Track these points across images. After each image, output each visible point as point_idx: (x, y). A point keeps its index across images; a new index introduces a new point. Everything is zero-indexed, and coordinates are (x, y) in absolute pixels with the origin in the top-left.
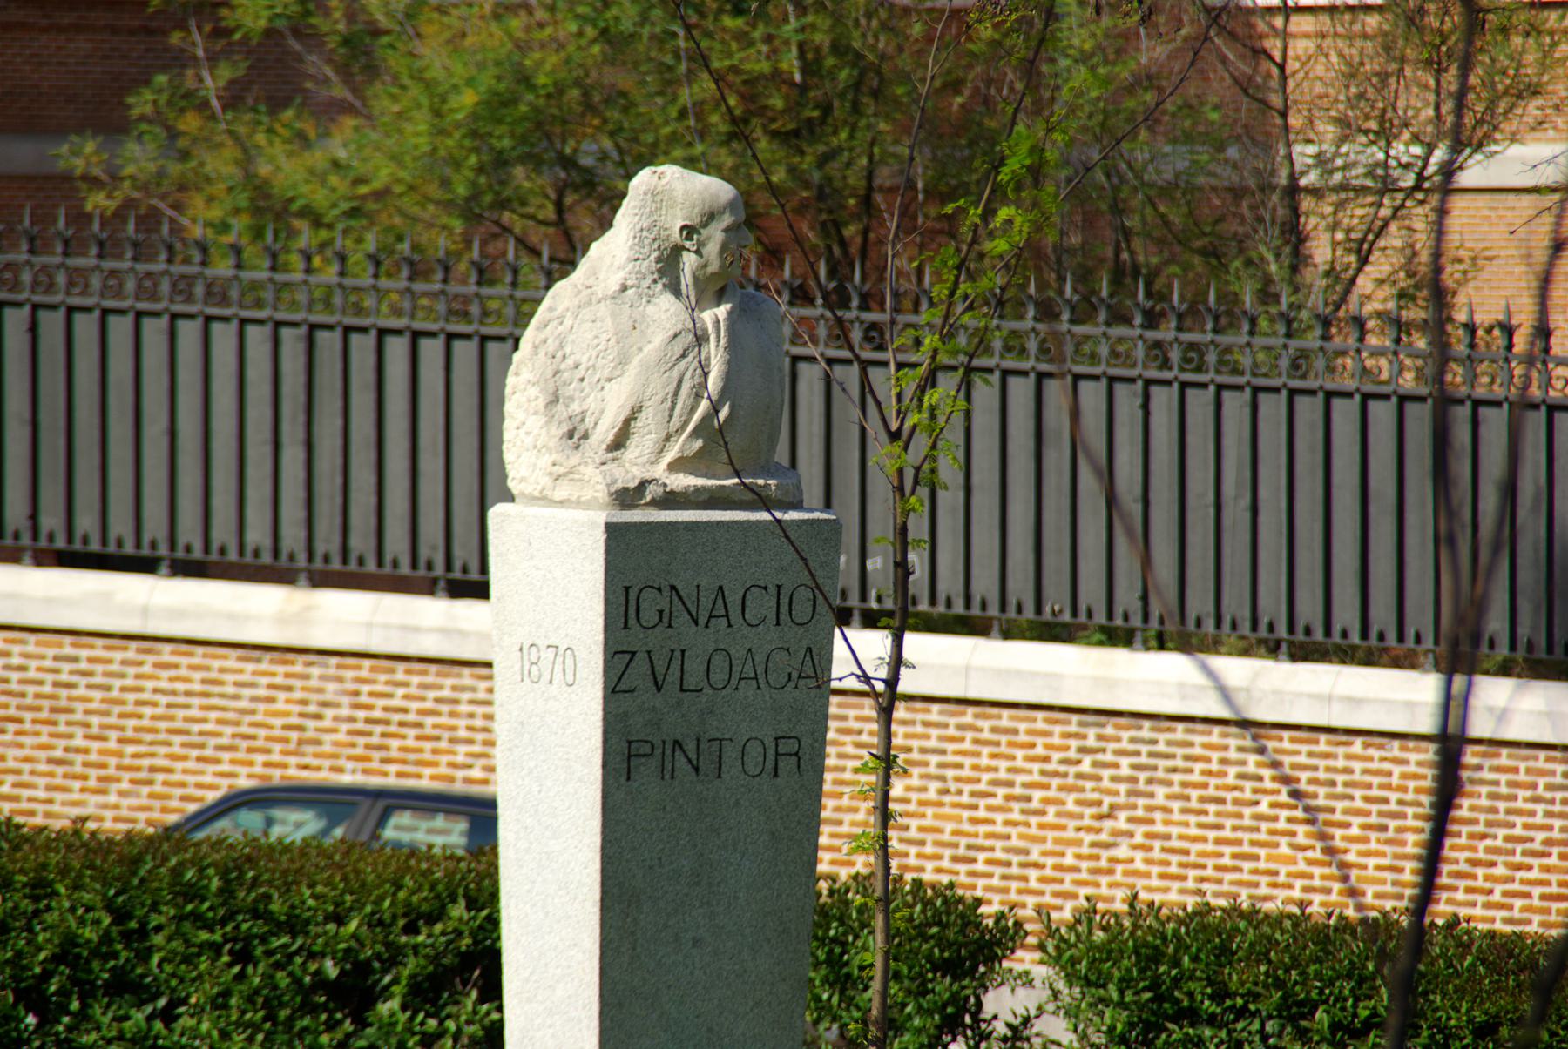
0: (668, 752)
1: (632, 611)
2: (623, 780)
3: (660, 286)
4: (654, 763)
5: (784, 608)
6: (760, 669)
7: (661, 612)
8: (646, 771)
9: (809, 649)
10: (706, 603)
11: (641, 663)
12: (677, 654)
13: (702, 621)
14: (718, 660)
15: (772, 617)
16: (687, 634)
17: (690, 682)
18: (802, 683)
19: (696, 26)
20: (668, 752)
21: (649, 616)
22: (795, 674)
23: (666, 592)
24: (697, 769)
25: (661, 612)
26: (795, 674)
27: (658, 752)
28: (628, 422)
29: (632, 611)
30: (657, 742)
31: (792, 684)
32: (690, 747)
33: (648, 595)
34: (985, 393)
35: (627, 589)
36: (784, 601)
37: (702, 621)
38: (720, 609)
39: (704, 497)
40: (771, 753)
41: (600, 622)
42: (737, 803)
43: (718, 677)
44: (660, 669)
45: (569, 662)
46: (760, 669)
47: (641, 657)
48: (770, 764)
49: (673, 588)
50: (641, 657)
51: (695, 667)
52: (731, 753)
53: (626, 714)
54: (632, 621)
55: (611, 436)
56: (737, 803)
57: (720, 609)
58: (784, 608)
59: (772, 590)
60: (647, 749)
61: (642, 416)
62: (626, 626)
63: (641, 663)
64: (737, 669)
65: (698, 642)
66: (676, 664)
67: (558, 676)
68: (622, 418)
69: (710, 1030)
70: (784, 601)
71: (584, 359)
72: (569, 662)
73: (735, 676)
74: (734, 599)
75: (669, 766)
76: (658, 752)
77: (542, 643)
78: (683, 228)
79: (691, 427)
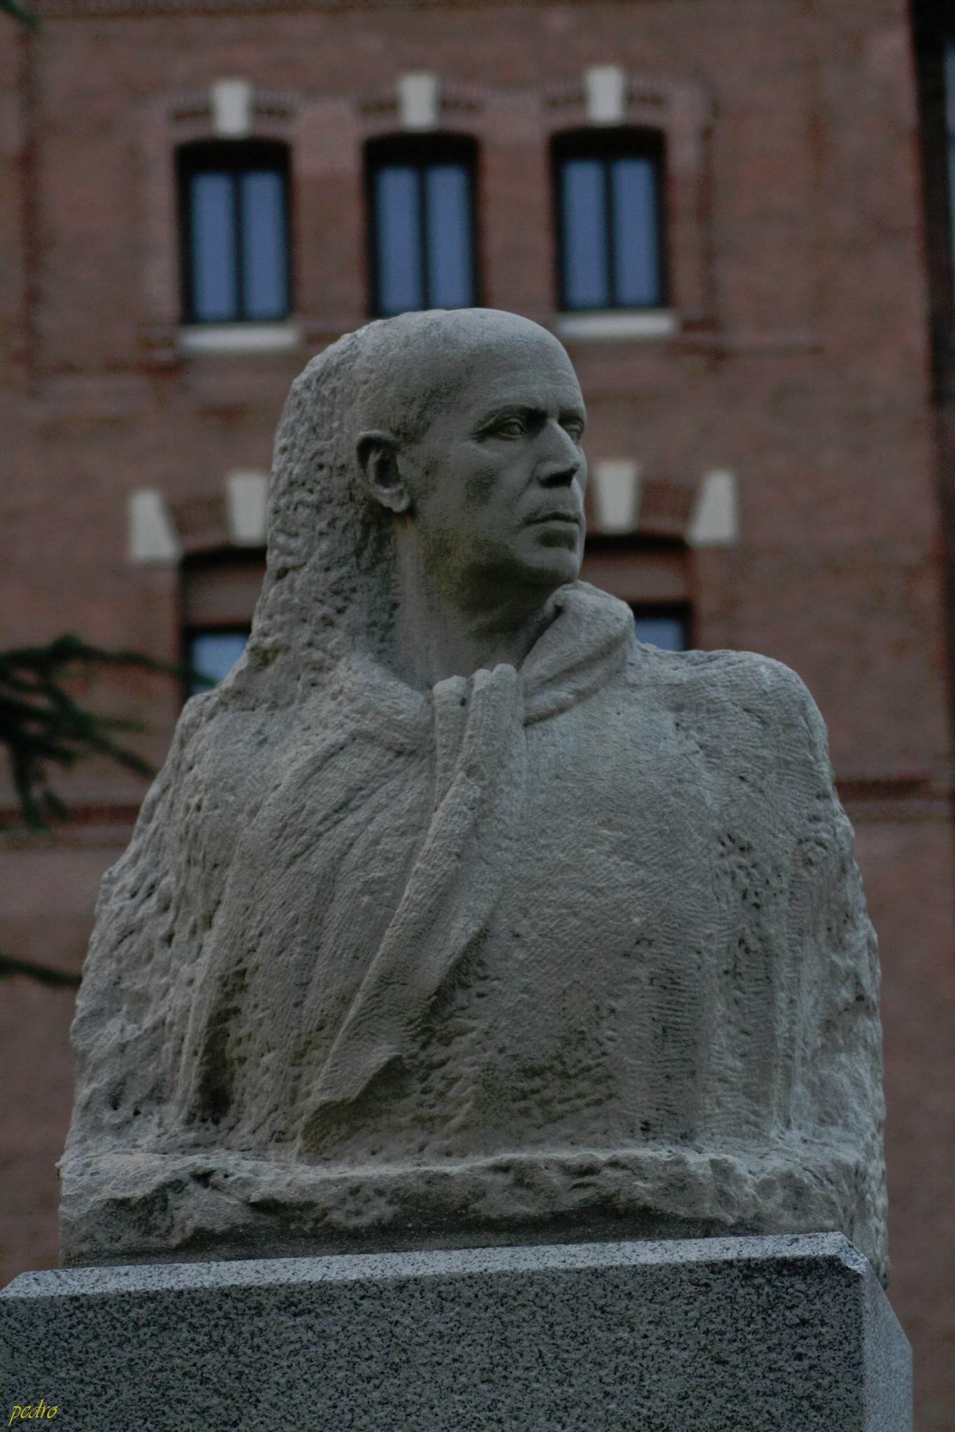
3: (336, 638)
39: (382, 1210)
78: (366, 446)
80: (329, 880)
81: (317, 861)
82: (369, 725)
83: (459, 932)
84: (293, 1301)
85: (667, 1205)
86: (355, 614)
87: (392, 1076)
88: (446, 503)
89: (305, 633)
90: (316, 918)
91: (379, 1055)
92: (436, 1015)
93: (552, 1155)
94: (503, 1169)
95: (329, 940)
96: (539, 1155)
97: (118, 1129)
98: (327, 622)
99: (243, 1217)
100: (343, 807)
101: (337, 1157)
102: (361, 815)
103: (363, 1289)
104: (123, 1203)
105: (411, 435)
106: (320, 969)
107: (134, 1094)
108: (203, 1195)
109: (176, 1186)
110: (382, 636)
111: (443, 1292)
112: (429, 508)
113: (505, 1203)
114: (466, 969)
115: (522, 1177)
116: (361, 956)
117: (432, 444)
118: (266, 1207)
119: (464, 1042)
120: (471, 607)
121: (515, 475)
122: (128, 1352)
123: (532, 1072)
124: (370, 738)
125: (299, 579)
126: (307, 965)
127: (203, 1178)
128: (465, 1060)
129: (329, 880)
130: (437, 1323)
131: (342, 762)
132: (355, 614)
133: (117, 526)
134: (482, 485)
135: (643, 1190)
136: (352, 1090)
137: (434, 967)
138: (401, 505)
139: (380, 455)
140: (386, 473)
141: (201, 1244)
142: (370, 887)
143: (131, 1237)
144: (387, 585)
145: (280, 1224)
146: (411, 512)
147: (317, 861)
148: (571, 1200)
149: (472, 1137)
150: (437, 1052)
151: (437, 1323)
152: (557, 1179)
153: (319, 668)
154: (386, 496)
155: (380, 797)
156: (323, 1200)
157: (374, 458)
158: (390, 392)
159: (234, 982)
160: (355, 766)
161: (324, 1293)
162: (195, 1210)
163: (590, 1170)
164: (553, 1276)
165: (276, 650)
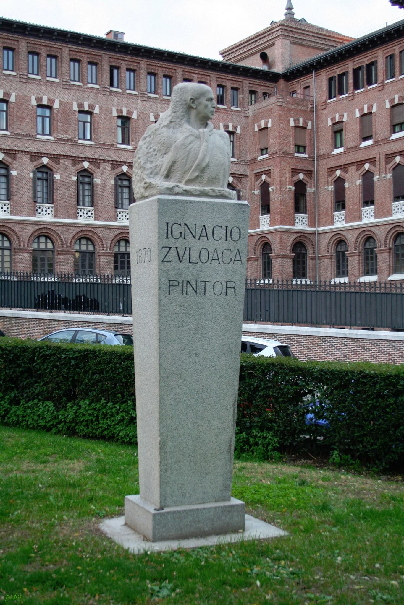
0: (185, 285)
1: (169, 232)
2: (167, 294)
3: (183, 122)
4: (179, 289)
5: (229, 235)
6: (220, 256)
7: (181, 233)
8: (176, 292)
9: (238, 250)
10: (199, 231)
11: (173, 252)
12: (188, 249)
13: (197, 237)
14: (203, 252)
15: (224, 237)
16: (191, 241)
17: (193, 260)
18: (236, 262)
19: (130, 439)
20: (185, 285)
21: (176, 234)
22: (233, 259)
23: (183, 226)
24: (196, 292)
25: (181, 233)
26: (233, 259)
27: (181, 285)
28: (171, 167)
29: (169, 232)
30: (180, 281)
31: (232, 263)
32: (193, 284)
33: (175, 226)
34: (39, 294)
35: (167, 223)
36: (229, 232)
37: (197, 237)
38: (204, 233)
39: (198, 193)
40: (224, 287)
41: (76, 31)
42: (212, 304)
43: (204, 258)
44: (181, 253)
45: (149, 253)
46: (220, 256)
47: (173, 249)
48: (224, 291)
49: (186, 224)
50: (173, 249)
51: (195, 255)
52: (209, 287)
53: (168, 270)
54: (170, 236)
55: (165, 173)
56: (212, 304)
57: (204, 233)
58: (229, 235)
59: (224, 228)
60: (176, 283)
61: (176, 165)
62: (167, 237)
63: (173, 252)
64: (211, 256)
65: (196, 245)
66: (187, 253)
67: (146, 259)
68: (169, 166)
69: (203, 386)
70: (229, 232)
71: (157, 148)
72: (149, 253)
73: (210, 258)
74: (209, 231)
75: (185, 290)
76: (181, 285)
77: (142, 248)
78: (191, 99)
79: (193, 168)
80: (189, 152)
81: (188, 149)
82: (192, 133)
83: (207, 161)
84: (191, 202)
85: (228, 196)
86: (185, 119)
87: (197, 177)
88: (201, 108)
89: (178, 120)
90: (188, 156)
91: (196, 174)
92: (203, 171)
93: (217, 188)
94: (211, 189)
95: (190, 160)
96: (216, 188)
97: (153, 178)
98: (182, 119)
99: (183, 191)
100: (190, 143)
101: (189, 185)
102: (193, 144)
103: (199, 202)
104: (168, 188)
105: (197, 99)
106: (188, 163)
107: (154, 173)
108: (177, 188)
109: (174, 187)
110: (188, 121)
111: (207, 203)
112: (199, 108)
113: (211, 193)
114: (207, 165)
115: (214, 191)
116: (194, 162)
117: (200, 100)
118: (185, 191)
119: (206, 174)
120: (201, 121)
121: (210, 106)
122: (173, 206)
123: (213, 178)
124: (192, 135)
125: (178, 113)
126: (186, 162)
127: (177, 186)
128: (206, 176)
129: (189, 152)
130: (206, 207)
131: (190, 138)
132: (185, 119)
133: (289, 122)
134: (206, 106)
135: (226, 194)
136: (193, 178)
137: (204, 165)
138: (195, 107)
139: (193, 100)
140: (193, 102)
141: (178, 194)
142: (195, 154)
143: (169, 192)
144: (189, 116)
145: (187, 193)
146: (196, 108)
147: (188, 149)
148: (218, 194)
149: (207, 184)
150: (203, 175)
151: (206, 207)
152: (217, 191)
153: (180, 125)
154: (193, 105)
155: (194, 143)
156: (192, 190)
157: (192, 101)
158: (195, 93)
159: (174, 162)
160: (191, 138)
161: (195, 202)
162: (177, 190)
163: (220, 191)
164: (219, 203)
165: (173, 122)
